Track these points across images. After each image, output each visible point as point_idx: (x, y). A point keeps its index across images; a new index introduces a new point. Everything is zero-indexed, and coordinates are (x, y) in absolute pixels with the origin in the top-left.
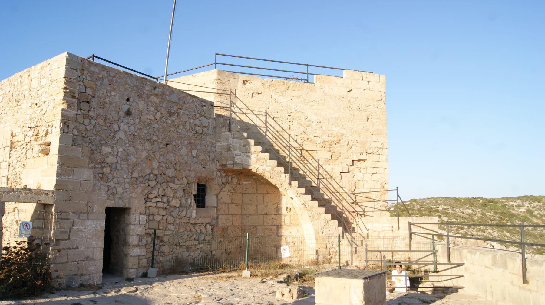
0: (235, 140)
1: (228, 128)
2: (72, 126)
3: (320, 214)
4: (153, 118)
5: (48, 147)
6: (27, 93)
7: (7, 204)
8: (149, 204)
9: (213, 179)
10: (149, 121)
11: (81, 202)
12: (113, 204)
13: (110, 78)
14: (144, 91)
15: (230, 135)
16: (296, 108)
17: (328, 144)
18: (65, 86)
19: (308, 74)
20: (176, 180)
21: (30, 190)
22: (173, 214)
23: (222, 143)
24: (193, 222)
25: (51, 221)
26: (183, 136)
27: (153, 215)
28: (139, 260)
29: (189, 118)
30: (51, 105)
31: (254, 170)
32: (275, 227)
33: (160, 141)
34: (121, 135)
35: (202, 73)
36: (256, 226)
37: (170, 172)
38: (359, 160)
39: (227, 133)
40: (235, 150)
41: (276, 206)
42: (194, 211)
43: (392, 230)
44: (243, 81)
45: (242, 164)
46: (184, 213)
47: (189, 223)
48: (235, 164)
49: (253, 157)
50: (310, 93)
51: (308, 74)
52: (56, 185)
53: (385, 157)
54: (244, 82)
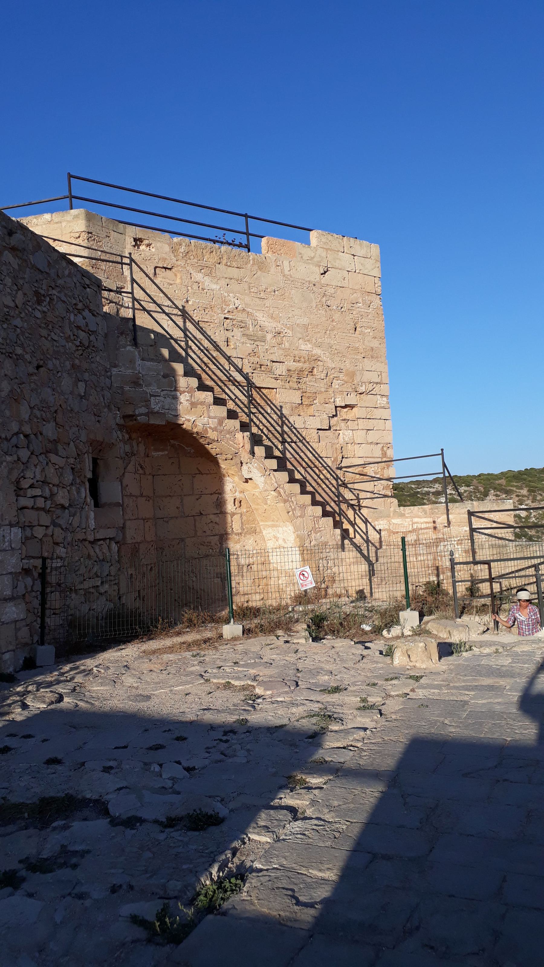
1: (130, 337)
3: (303, 507)
4: (12, 305)
8: (23, 502)
10: (6, 310)
15: (137, 353)
16: (237, 303)
17: (295, 376)
19: (248, 234)
20: (60, 447)
22: (61, 522)
24: (91, 538)
26: (62, 350)
27: (31, 527)
28: (17, 630)
29: (68, 311)
31: (187, 426)
32: (217, 538)
33: (28, 357)
35: (47, 216)
36: (182, 540)
37: (49, 430)
38: (346, 406)
40: (149, 385)
42: (92, 515)
43: (435, 528)
44: (135, 240)
46: (77, 519)
47: (85, 540)
48: (151, 413)
49: (184, 399)
50: (259, 273)
51: (248, 234)
53: (385, 399)
54: (138, 241)
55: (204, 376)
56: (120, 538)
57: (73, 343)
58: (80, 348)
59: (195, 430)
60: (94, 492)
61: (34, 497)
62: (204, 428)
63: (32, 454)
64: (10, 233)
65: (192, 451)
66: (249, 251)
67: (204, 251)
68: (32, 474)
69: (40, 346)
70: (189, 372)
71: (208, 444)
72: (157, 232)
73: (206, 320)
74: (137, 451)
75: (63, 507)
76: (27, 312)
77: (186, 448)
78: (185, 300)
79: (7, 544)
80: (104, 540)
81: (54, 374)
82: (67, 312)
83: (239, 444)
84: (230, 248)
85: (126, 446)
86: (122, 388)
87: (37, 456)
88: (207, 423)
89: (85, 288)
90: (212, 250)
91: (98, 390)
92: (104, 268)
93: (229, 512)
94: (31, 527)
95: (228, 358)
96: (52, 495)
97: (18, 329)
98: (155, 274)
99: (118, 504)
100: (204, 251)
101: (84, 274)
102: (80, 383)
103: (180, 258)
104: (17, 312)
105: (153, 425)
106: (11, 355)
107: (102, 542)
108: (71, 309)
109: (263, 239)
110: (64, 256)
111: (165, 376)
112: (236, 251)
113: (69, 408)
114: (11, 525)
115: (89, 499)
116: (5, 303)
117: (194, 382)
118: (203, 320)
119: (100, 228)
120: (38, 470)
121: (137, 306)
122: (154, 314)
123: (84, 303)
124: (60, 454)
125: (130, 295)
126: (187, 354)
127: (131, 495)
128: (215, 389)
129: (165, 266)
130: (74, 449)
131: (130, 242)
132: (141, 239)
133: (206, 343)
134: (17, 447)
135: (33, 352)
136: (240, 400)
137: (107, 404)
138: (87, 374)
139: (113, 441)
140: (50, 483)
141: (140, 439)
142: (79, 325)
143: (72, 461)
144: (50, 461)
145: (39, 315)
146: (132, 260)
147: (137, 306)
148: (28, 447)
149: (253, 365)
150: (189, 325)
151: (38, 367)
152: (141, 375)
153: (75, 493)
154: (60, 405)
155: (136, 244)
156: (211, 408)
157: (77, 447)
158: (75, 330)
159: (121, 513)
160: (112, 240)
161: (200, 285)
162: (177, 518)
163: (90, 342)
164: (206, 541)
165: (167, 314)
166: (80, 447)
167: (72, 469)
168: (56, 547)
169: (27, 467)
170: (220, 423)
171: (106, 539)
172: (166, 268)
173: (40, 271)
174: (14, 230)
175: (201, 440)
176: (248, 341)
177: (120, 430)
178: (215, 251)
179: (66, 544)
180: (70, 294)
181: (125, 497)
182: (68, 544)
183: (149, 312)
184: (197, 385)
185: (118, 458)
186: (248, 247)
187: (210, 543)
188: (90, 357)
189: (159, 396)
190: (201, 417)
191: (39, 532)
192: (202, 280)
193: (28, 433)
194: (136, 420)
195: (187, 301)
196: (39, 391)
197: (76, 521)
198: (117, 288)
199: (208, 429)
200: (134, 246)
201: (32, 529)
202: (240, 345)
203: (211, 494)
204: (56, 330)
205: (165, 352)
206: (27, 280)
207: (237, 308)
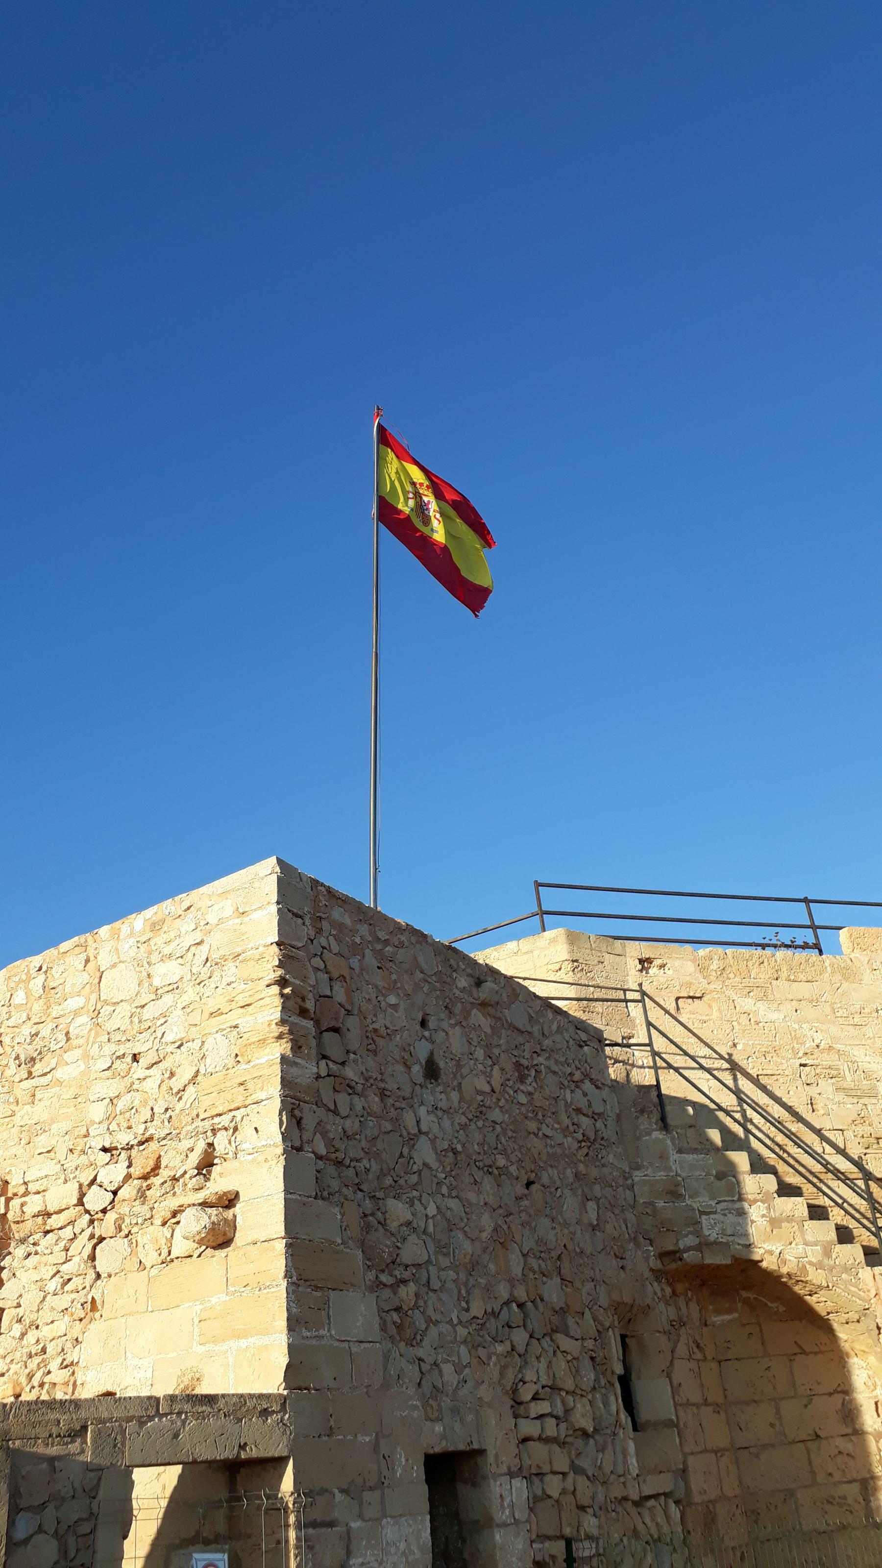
0: (690, 1157)
1: (655, 1116)
2: (309, 1122)
5: (229, 1214)
6: (81, 1025)
7: (138, 1474)
8: (529, 1428)
9: (647, 1309)
10: (480, 1098)
11: (360, 1438)
12: (443, 1437)
13: (379, 947)
14: (457, 993)
15: (669, 1142)
16: (818, 1037)
18: (280, 972)
19: (814, 927)
20: (571, 1321)
21: (210, 1399)
23: (649, 1172)
24: (635, 1496)
25: (280, 1544)
26: (559, 1151)
27: (540, 1475)
29: (562, 1086)
30: (219, 1050)
32: (856, 1487)
33: (513, 1169)
34: (424, 1152)
35: (512, 945)
36: (790, 1493)
39: (657, 1135)
41: (838, 1398)
42: (631, 1447)
44: (641, 961)
45: (727, 1244)
46: (608, 1456)
47: (625, 1499)
48: (704, 1245)
49: (756, 1213)
50: (845, 985)
51: (814, 927)
52: (288, 1366)
54: (645, 963)
55: (781, 1167)
56: (680, 1494)
57: (573, 1138)
58: (583, 1144)
59: (784, 1270)
60: (629, 1404)
61: (541, 1417)
62: (800, 1265)
63: (531, 1337)
64: (479, 983)
65: (782, 1309)
66: (821, 953)
67: (750, 964)
68: (536, 1374)
69: (529, 1150)
70: (759, 1166)
71: (810, 1295)
72: (673, 944)
73: (769, 1072)
74: (687, 1317)
75: (585, 1434)
76: (507, 1097)
77: (770, 1304)
78: (730, 1043)
79: (507, 1512)
80: (655, 1496)
81: (551, 1193)
82: (561, 1088)
83: (869, 1291)
84: (789, 952)
85: (669, 1308)
86: (652, 1204)
87: (538, 1339)
88: (804, 1255)
89: (581, 1046)
90: (761, 960)
91: (617, 1211)
92: (601, 1010)
93: (870, 1430)
94: (540, 1475)
95: (818, 1132)
96: (567, 1411)
97: (498, 1126)
98: (678, 1009)
99: (670, 1424)
100: (750, 964)
101: (579, 1025)
102: (590, 1203)
103: (713, 978)
104: (494, 1100)
105: (709, 1266)
106: (490, 1170)
107: (652, 1502)
108: (566, 1083)
109: (841, 931)
110: (546, 1002)
111: (720, 1176)
112: (801, 955)
113: (578, 1250)
114: (511, 1475)
115: (624, 1416)
116: (478, 1088)
117: (769, 1182)
118: (765, 1072)
119: (588, 951)
120: (543, 1366)
121: (660, 1063)
122: (685, 1073)
123: (583, 1070)
124: (572, 1334)
125: (648, 1048)
126: (747, 1131)
127: (688, 1404)
128: (804, 1190)
129: (691, 994)
130: (592, 1322)
131: (633, 965)
132: (649, 958)
133: (777, 1111)
134: (509, 1327)
135: (520, 1160)
136: (851, 1205)
137: (633, 1235)
138: (597, 1187)
139: (648, 1301)
140: (560, 1389)
141: (690, 1293)
142: (579, 1106)
143: (590, 1344)
144: (558, 1348)
145: (523, 1099)
146: (644, 994)
147: (660, 1063)
148: (524, 1326)
149: (863, 1140)
150: (745, 1085)
151: (529, 1184)
152: (679, 1179)
153: (601, 1406)
154: (565, 1246)
155: (643, 967)
156: (806, 1227)
157: (595, 1319)
158: (574, 1115)
159: (677, 1440)
160: (608, 968)
161: (751, 1016)
162: (773, 1446)
163: (597, 1131)
164: (836, 1495)
165: (709, 1071)
166: (601, 1318)
167: (592, 1359)
168: (582, 1514)
169: (526, 1363)
170: (827, 1253)
171: (659, 1495)
172: (693, 998)
173: (519, 1030)
174: (482, 978)
175: (797, 1288)
176: (846, 1099)
177: (657, 1279)
178: (766, 961)
179: (597, 1508)
180: (562, 1059)
181: (680, 1408)
182: (600, 1508)
183: (676, 1070)
184: (776, 1187)
185: (660, 1332)
186: (817, 947)
187: (845, 1498)
188: (600, 1156)
189: (715, 1213)
190: (791, 1244)
191: (554, 1485)
192: (754, 1009)
193: (522, 1300)
194: (681, 1260)
195: (735, 1045)
196: (533, 1224)
197: (607, 1460)
198: (623, 1038)
199: (808, 1266)
200: (641, 971)
201: (542, 1481)
202: (834, 1107)
203: (830, 1394)
204: (549, 1120)
205: (715, 1135)
206: (503, 1048)
207: (818, 1046)
